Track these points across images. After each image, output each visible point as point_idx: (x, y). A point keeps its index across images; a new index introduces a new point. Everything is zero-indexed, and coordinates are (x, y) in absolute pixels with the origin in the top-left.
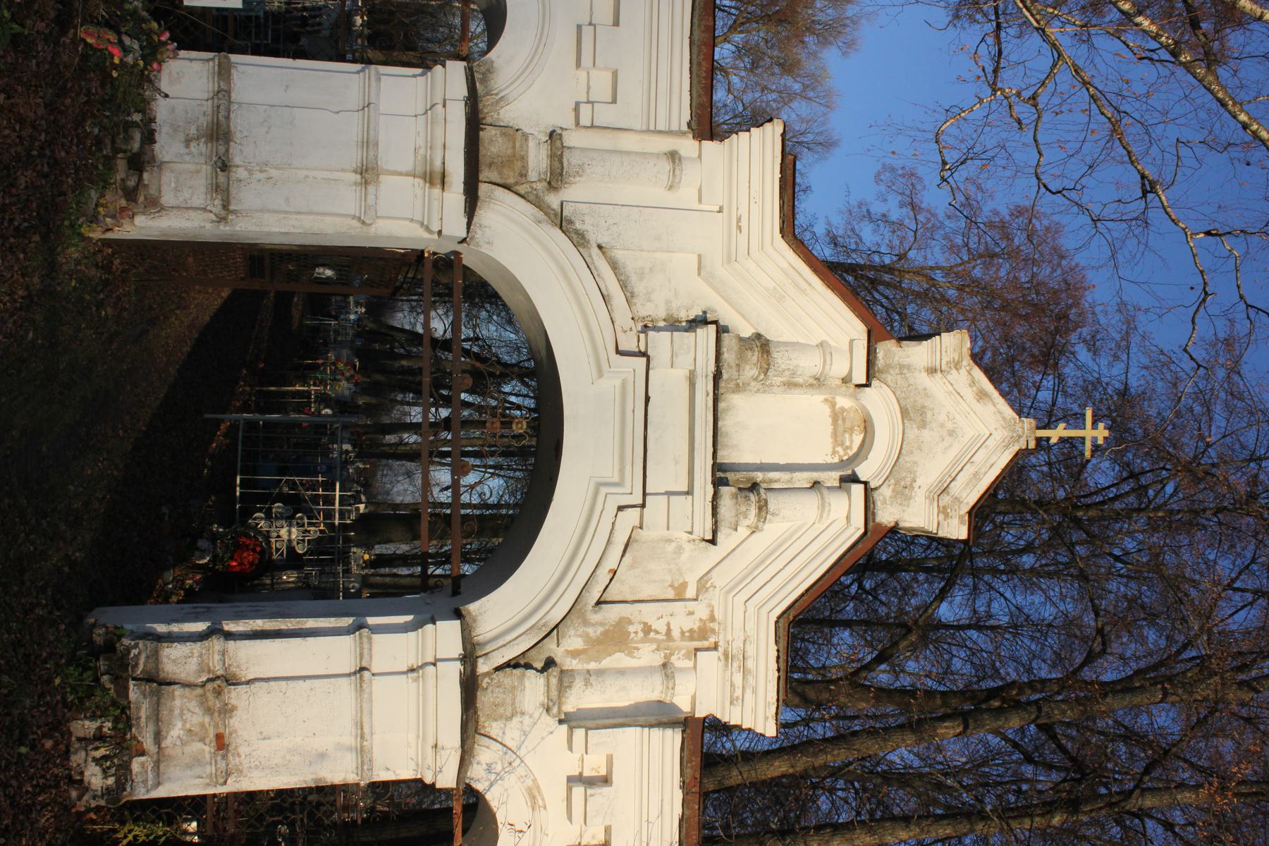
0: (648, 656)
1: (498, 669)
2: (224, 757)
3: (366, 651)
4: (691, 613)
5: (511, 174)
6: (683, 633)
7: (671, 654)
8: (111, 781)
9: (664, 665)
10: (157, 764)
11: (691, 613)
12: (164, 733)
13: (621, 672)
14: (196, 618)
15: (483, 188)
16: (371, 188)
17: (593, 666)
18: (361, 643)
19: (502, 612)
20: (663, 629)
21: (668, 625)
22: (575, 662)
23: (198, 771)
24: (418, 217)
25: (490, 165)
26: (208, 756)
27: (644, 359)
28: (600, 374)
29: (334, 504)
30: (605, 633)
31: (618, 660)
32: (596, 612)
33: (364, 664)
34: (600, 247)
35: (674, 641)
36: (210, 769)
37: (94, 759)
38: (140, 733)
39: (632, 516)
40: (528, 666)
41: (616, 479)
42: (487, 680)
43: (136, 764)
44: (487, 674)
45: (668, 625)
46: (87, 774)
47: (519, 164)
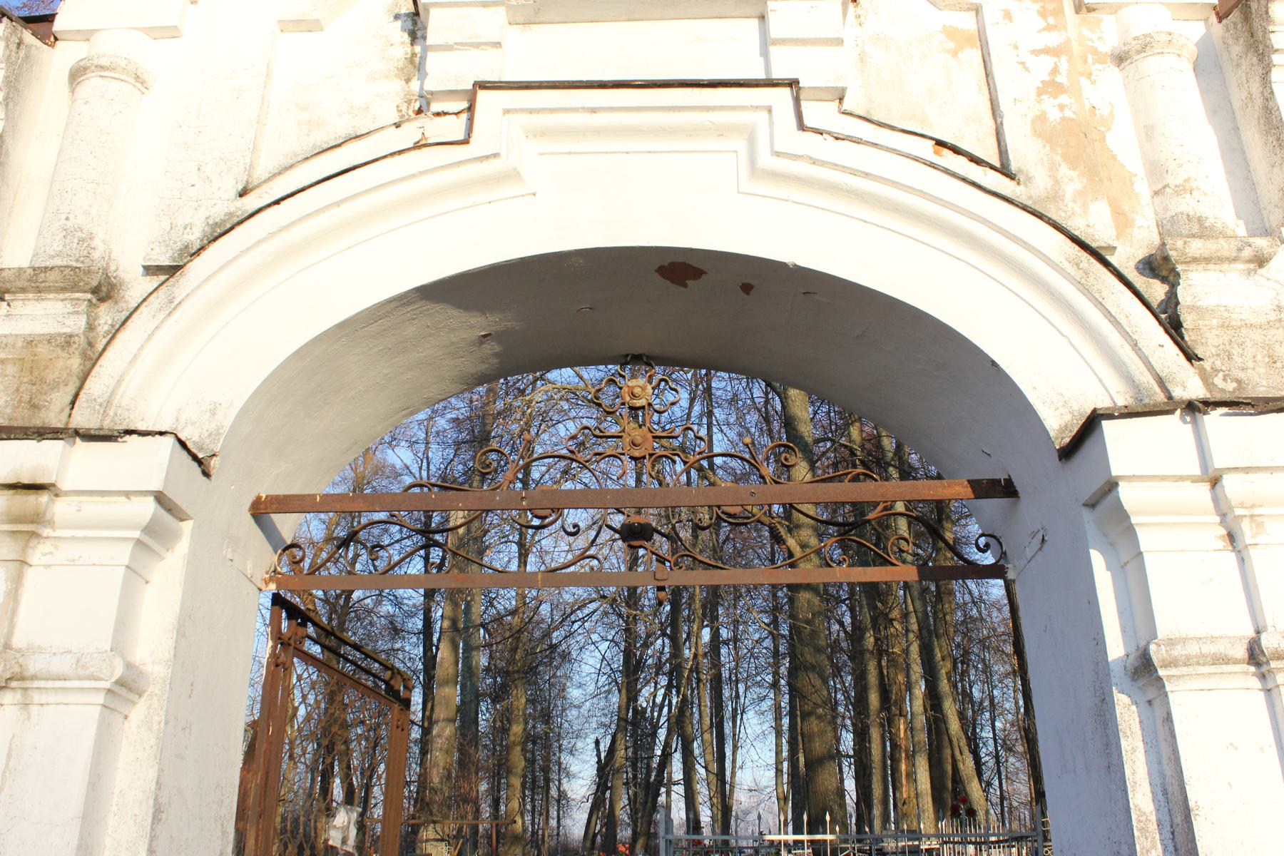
0: (1106, 90)
1: (1190, 357)
3: (1209, 649)
4: (1008, 15)
5: (60, 364)
6: (1049, 28)
7: (1095, 52)
9: (1120, 59)
11: (1008, 15)
13: (1148, 133)
15: (81, 419)
16: (34, 665)
17: (1143, 188)
18: (1188, 661)
19: (1053, 355)
20: (1048, 62)
21: (1036, 52)
22: (1139, 221)
24: (124, 553)
25: (35, 407)
27: (482, 95)
28: (513, 176)
29: (809, 833)
30: (1073, 162)
31: (1123, 143)
32: (1029, 179)
33: (1241, 652)
34: (242, 194)
35: (1068, 42)
39: (815, 113)
40: (1172, 300)
41: (741, 144)
42: (1218, 380)
44: (1206, 378)
45: (1036, 52)
47: (42, 350)
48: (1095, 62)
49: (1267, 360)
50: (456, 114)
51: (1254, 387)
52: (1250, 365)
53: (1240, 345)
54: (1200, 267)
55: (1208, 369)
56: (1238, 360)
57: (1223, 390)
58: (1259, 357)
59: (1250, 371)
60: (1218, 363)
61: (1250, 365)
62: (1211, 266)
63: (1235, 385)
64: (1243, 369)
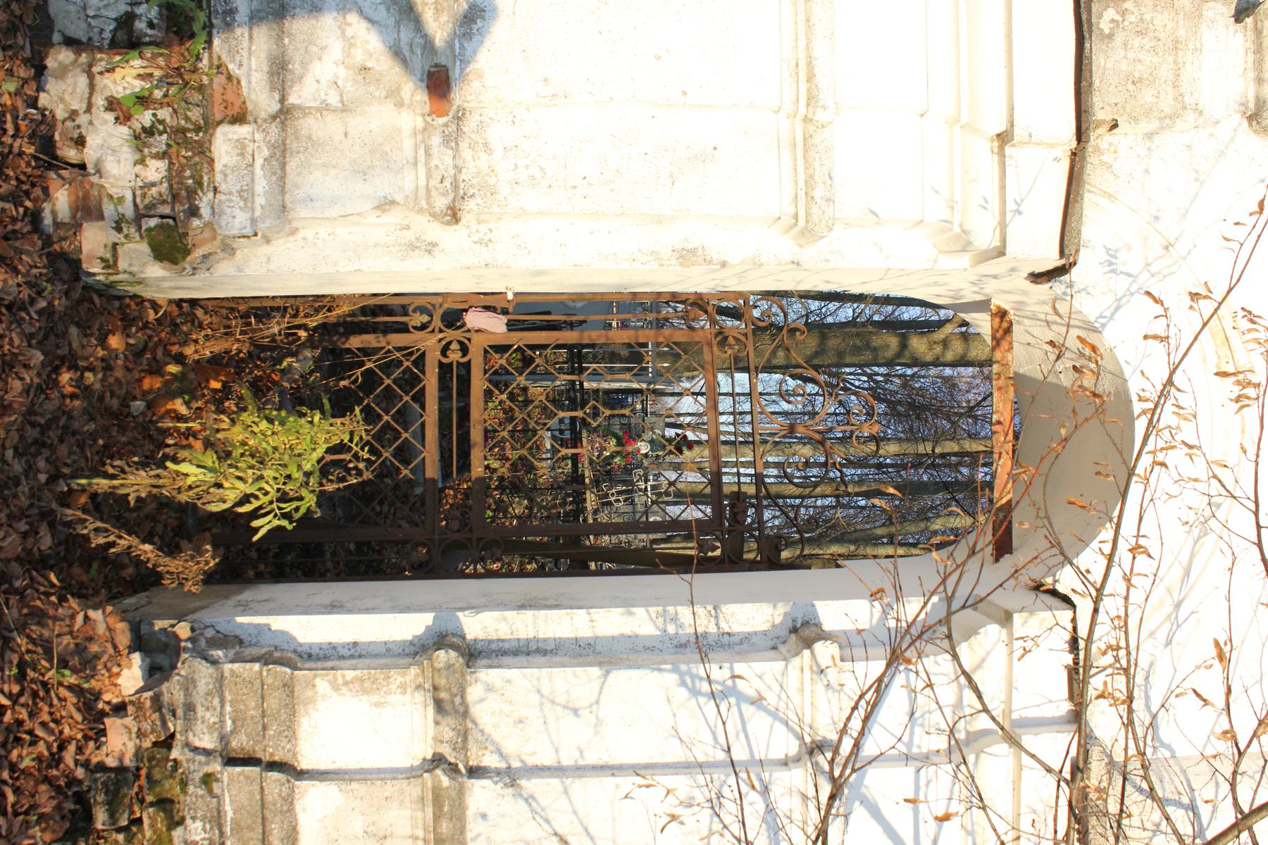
2: (452, 140)
8: (156, 170)
10: (280, 154)
12: (295, 66)
14: (241, 625)
23: (382, 185)
26: (408, 144)
36: (411, 180)
37: (112, 104)
38: (233, 52)
43: (226, 143)
46: (92, 141)
48: (161, 307)
49: (1137, 75)
50: (1231, 570)
51: (1105, 52)
52: (1131, 55)
53: (1154, 49)
54: (1250, 44)
55: (1126, 5)
56: (1137, 42)
57: (1100, 16)
58: (1139, 67)
59: (1123, 53)
60: (1132, 18)
61: (1131, 55)
62: (1251, 57)
63: (1107, 31)
64: (1125, 45)
